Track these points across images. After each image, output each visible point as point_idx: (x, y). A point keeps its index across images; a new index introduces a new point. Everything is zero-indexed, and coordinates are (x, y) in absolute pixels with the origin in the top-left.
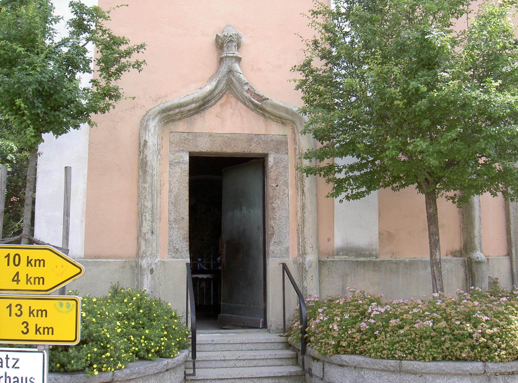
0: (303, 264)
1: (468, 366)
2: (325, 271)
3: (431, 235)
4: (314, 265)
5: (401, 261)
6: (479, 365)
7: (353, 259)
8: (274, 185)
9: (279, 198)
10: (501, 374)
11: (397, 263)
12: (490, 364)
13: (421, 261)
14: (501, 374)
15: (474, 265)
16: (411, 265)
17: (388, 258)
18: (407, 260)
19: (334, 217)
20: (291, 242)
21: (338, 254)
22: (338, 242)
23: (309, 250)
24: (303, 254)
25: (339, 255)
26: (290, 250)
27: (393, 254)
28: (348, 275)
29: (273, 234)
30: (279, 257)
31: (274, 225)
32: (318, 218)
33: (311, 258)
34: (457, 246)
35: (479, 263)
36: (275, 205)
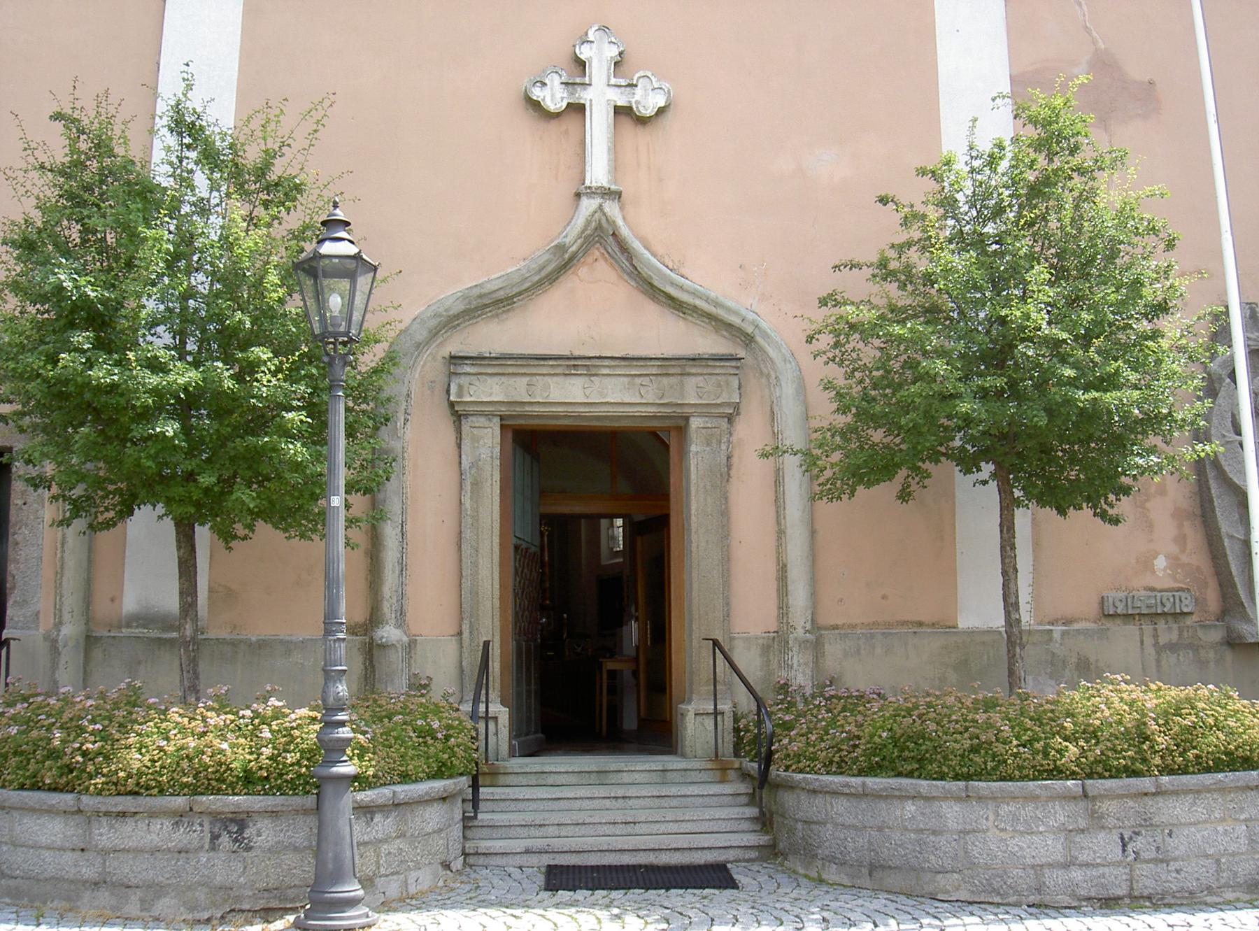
0: (57, 641)
1: (55, 799)
2: (97, 654)
3: (1004, 573)
4: (70, 644)
5: (241, 641)
6: (69, 798)
7: (155, 634)
8: (20, 502)
9: (26, 525)
10: (107, 814)
11: (234, 644)
12: (85, 798)
13: (281, 641)
14: (107, 814)
15: (375, 652)
16: (260, 648)
17: (225, 634)
18: (254, 639)
19: (124, 558)
20: (42, 602)
21: (128, 626)
22: (130, 604)
23: (66, 617)
24: (59, 624)
25: (131, 627)
26: (41, 616)
27: (235, 627)
28: (139, 663)
29: (14, 588)
30: (22, 628)
31: (15, 572)
32: (90, 561)
33: (70, 630)
34: (360, 616)
35: (383, 647)
36: (18, 538)
